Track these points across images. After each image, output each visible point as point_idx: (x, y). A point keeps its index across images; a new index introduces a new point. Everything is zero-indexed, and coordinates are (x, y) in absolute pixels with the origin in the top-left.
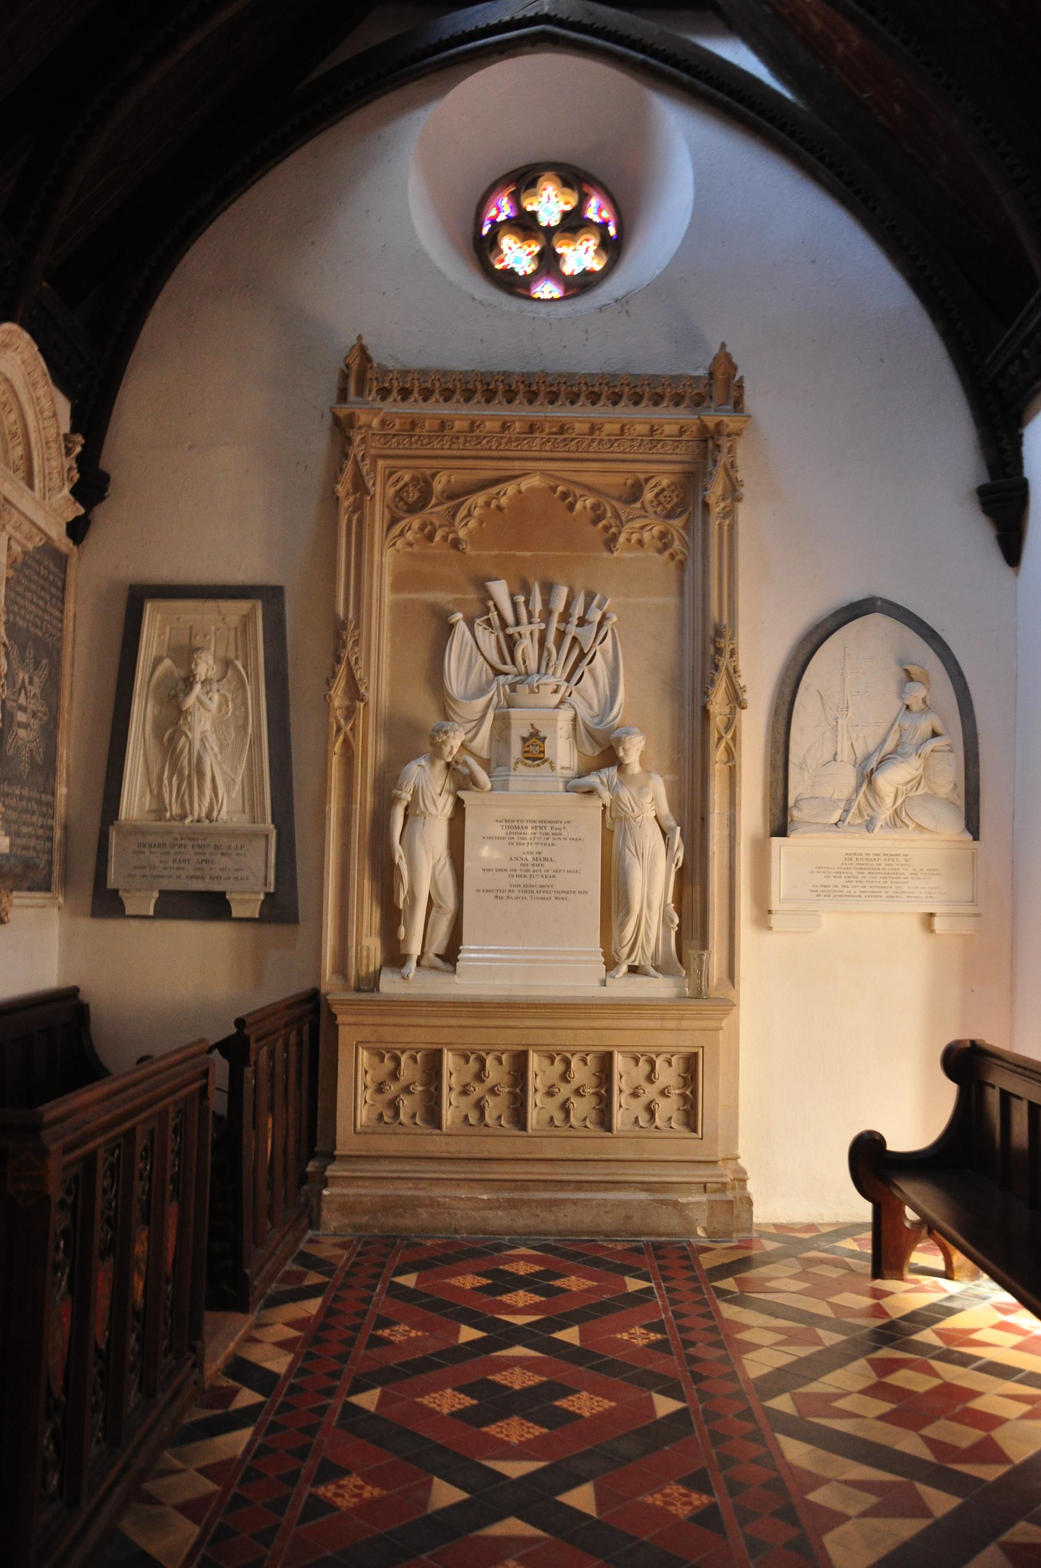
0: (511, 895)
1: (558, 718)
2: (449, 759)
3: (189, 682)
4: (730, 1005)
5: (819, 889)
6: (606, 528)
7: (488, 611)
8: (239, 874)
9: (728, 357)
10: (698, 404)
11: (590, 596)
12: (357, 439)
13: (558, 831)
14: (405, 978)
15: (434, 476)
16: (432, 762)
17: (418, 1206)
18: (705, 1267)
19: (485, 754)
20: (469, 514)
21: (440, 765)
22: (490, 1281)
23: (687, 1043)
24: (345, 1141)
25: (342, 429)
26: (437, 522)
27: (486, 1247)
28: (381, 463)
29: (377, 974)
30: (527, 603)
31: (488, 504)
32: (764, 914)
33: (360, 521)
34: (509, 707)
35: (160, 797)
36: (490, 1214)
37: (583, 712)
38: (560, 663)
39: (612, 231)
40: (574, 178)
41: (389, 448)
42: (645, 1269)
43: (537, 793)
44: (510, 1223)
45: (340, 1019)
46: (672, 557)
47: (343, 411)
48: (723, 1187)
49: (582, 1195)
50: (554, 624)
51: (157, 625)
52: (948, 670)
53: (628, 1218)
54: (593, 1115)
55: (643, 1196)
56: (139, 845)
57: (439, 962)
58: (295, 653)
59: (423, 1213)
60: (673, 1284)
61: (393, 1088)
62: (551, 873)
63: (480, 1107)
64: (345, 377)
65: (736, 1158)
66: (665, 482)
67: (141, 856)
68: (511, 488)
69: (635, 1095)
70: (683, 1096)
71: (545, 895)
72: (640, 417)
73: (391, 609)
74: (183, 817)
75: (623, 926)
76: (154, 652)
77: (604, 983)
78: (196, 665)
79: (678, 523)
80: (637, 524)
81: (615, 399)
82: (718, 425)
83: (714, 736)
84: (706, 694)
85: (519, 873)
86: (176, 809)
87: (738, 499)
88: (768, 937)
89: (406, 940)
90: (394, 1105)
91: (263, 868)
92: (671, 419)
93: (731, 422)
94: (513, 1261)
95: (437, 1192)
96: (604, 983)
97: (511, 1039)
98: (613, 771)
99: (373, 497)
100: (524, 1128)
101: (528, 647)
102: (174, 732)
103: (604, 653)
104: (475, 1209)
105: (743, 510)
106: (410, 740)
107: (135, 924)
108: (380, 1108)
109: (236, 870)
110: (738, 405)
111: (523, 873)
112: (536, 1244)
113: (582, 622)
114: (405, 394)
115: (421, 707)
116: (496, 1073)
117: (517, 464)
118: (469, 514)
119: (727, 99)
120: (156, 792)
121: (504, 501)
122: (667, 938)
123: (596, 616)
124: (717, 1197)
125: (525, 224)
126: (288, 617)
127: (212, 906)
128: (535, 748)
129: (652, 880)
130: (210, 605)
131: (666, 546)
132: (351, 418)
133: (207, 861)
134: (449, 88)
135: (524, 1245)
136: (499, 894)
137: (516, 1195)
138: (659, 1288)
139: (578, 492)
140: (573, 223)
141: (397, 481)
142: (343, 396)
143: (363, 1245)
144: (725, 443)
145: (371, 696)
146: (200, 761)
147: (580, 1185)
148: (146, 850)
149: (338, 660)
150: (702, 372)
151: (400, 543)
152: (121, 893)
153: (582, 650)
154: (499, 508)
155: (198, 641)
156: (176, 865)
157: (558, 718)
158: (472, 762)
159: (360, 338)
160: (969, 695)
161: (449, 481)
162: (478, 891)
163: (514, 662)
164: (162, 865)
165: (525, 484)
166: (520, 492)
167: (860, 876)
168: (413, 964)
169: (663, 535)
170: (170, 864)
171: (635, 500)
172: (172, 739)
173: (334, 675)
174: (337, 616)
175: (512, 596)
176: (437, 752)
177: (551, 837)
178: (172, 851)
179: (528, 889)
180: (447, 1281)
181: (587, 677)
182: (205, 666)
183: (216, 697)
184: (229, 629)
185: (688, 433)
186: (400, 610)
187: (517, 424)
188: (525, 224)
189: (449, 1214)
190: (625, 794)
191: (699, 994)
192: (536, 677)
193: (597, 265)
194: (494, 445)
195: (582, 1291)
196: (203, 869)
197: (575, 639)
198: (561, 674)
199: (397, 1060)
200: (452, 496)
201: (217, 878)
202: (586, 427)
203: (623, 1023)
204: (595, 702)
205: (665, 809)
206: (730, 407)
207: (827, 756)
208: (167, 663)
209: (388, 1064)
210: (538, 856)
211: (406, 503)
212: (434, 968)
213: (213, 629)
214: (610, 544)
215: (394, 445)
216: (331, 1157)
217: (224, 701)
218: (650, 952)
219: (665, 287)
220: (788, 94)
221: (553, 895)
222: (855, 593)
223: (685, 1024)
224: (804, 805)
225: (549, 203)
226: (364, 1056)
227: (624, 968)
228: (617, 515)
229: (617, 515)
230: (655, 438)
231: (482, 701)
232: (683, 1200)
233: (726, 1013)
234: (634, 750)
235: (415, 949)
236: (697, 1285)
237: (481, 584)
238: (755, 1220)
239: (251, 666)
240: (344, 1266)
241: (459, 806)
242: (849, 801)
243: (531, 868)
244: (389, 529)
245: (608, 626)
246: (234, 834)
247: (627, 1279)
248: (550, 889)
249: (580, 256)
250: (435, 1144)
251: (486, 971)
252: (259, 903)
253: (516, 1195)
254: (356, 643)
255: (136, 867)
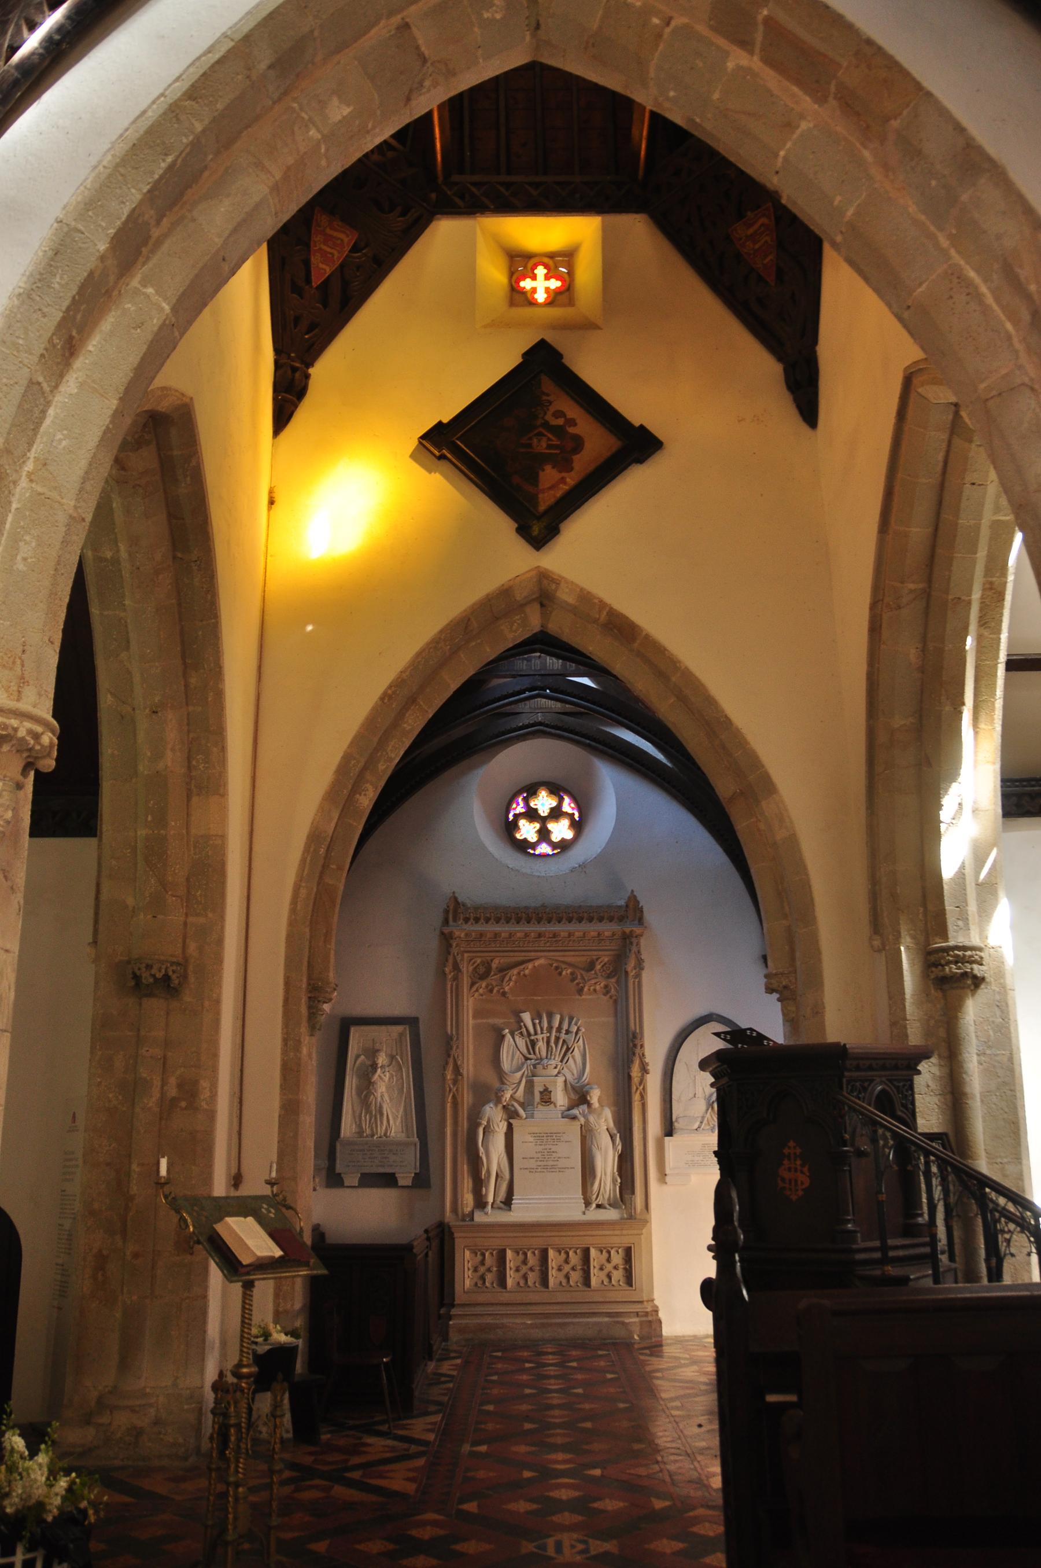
1: (558, 1082)
3: (374, 1067)
4: (646, 1222)
6: (578, 984)
7: (521, 1028)
9: (635, 897)
10: (621, 921)
11: (571, 1019)
12: (454, 945)
14: (486, 1214)
16: (496, 1105)
19: (522, 1100)
20: (510, 979)
21: (500, 1106)
23: (626, 1241)
24: (460, 1297)
25: (446, 939)
26: (494, 983)
28: (466, 955)
29: (472, 1213)
30: (540, 1023)
31: (519, 973)
32: (663, 1176)
33: (457, 986)
34: (533, 1076)
35: (360, 1126)
37: (569, 1077)
38: (558, 1052)
39: (576, 817)
40: (556, 790)
43: (548, 1118)
45: (456, 1235)
46: (611, 997)
47: (446, 930)
48: (646, 1314)
49: (577, 1320)
50: (554, 1033)
51: (357, 1039)
54: (581, 1280)
55: (606, 1319)
57: (502, 1205)
58: (427, 1051)
61: (482, 1269)
63: (525, 1277)
64: (446, 912)
65: (653, 1300)
66: (606, 960)
68: (530, 966)
69: (601, 1269)
70: (625, 1269)
72: (592, 929)
74: (373, 1136)
75: (592, 1184)
76: (355, 1052)
77: (584, 1213)
79: (613, 980)
80: (593, 981)
81: (580, 920)
82: (631, 931)
83: (634, 1088)
84: (629, 1068)
86: (368, 1131)
87: (643, 969)
88: (665, 1187)
89: (486, 1195)
90: (483, 1278)
92: (608, 929)
93: (638, 930)
95: (505, 1321)
96: (584, 1213)
97: (539, 1242)
98: (585, 1107)
100: (547, 1287)
101: (541, 1045)
103: (579, 1047)
105: (645, 975)
106: (485, 1094)
107: (348, 1190)
108: (475, 1280)
110: (641, 921)
113: (568, 1032)
114: (477, 920)
115: (489, 1076)
116: (533, 1260)
117: (533, 954)
118: (510, 979)
121: (527, 972)
122: (615, 1191)
123: (574, 1029)
124: (644, 1319)
125: (531, 815)
126: (421, 1032)
127: (388, 1180)
128: (546, 1097)
129: (606, 1161)
130: (383, 1028)
131: (607, 992)
132: (451, 933)
134: (490, 761)
136: (531, 1170)
137: (545, 1321)
139: (564, 966)
140: (556, 813)
142: (446, 922)
144: (634, 940)
145: (465, 1073)
146: (381, 1107)
147: (575, 1315)
149: (449, 1056)
150: (622, 903)
151: (476, 994)
154: (525, 975)
155: (377, 1046)
157: (558, 1082)
158: (516, 1104)
163: (534, 1053)
165: (537, 963)
168: (490, 1207)
169: (606, 986)
171: (592, 970)
172: (366, 1096)
173: (447, 1063)
174: (446, 1032)
175: (533, 1020)
176: (498, 1100)
179: (545, 1167)
181: (571, 1060)
182: (382, 1059)
183: (388, 1074)
186: (476, 1027)
188: (531, 815)
190: (591, 1119)
191: (631, 1217)
192: (545, 1061)
193: (569, 835)
194: (521, 944)
197: (564, 1041)
198: (558, 1058)
199: (483, 1255)
202: (566, 934)
203: (594, 1233)
204: (575, 1072)
205: (611, 1124)
206: (636, 922)
207: (691, 1095)
208: (363, 1057)
209: (479, 1257)
212: (500, 1208)
214: (580, 991)
216: (453, 1306)
217: (391, 1076)
218: (607, 1196)
219: (602, 859)
220: (660, 757)
222: (701, 1011)
223: (625, 1232)
224: (680, 1120)
225: (544, 802)
226: (467, 1253)
227: (594, 1206)
228: (583, 978)
229: (583, 978)
231: (519, 1074)
232: (627, 1321)
233: (644, 1226)
234: (595, 1096)
235: (490, 1199)
237: (517, 1014)
238: (664, 1333)
241: (510, 1127)
242: (703, 1117)
244: (471, 987)
245: (580, 1034)
246: (399, 1144)
249: (561, 830)
250: (505, 1297)
251: (522, 1212)
253: (545, 1321)
254: (457, 1047)
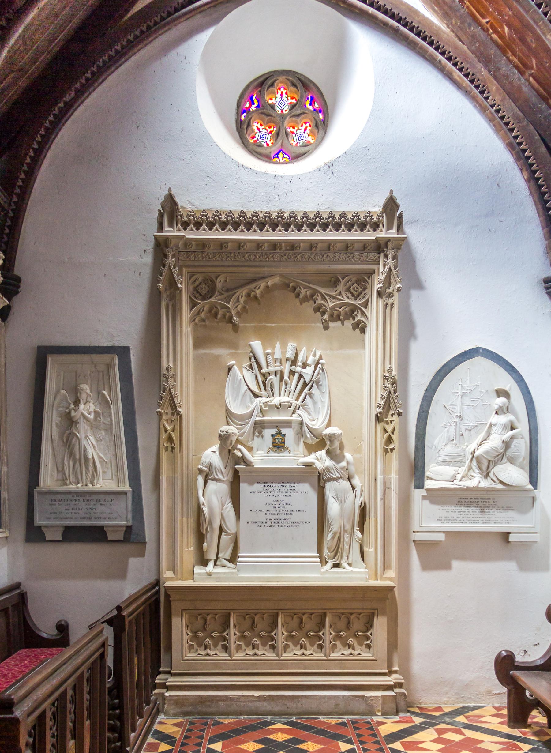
0: (267, 524)
2: (230, 448)
5: (443, 519)
8: (111, 516)
12: (170, 255)
13: (293, 488)
15: (217, 278)
17: (219, 701)
18: (383, 735)
22: (263, 746)
27: (258, 723)
31: (248, 295)
36: (258, 704)
41: (190, 260)
42: (349, 737)
44: (271, 709)
52: (522, 390)
53: (337, 705)
56: (52, 500)
59: (221, 704)
60: (366, 746)
62: (289, 512)
64: (161, 215)
67: (54, 507)
71: (286, 524)
73: (194, 359)
78: (80, 394)
85: (271, 512)
91: (125, 512)
94: (275, 733)
99: (181, 291)
102: (70, 434)
104: (252, 701)
109: (109, 513)
111: (273, 512)
112: (286, 721)
119: (396, 24)
120: (60, 469)
133: (92, 509)
135: (279, 722)
136: (259, 524)
138: (359, 749)
141: (195, 281)
142: (161, 227)
143: (189, 725)
148: (57, 503)
152: (43, 529)
153: (305, 381)
156: (73, 511)
159: (170, 189)
160: (533, 405)
161: (226, 281)
162: (248, 523)
164: (67, 511)
166: (267, 287)
167: (467, 511)
170: (71, 511)
177: (289, 491)
178: (72, 503)
179: (277, 521)
180: (239, 746)
184: (99, 372)
185: (369, 248)
187: (266, 245)
189: (236, 704)
194: (252, 257)
195: (315, 751)
196: (90, 513)
200: (228, 290)
201: (98, 518)
210: (282, 502)
211: (200, 295)
213: (89, 372)
215: (193, 258)
221: (290, 524)
230: (349, 251)
236: (380, 746)
239: (113, 394)
240: (180, 738)
243: (278, 509)
247: (340, 743)
248: (289, 521)
252: (123, 532)
255: (51, 513)
